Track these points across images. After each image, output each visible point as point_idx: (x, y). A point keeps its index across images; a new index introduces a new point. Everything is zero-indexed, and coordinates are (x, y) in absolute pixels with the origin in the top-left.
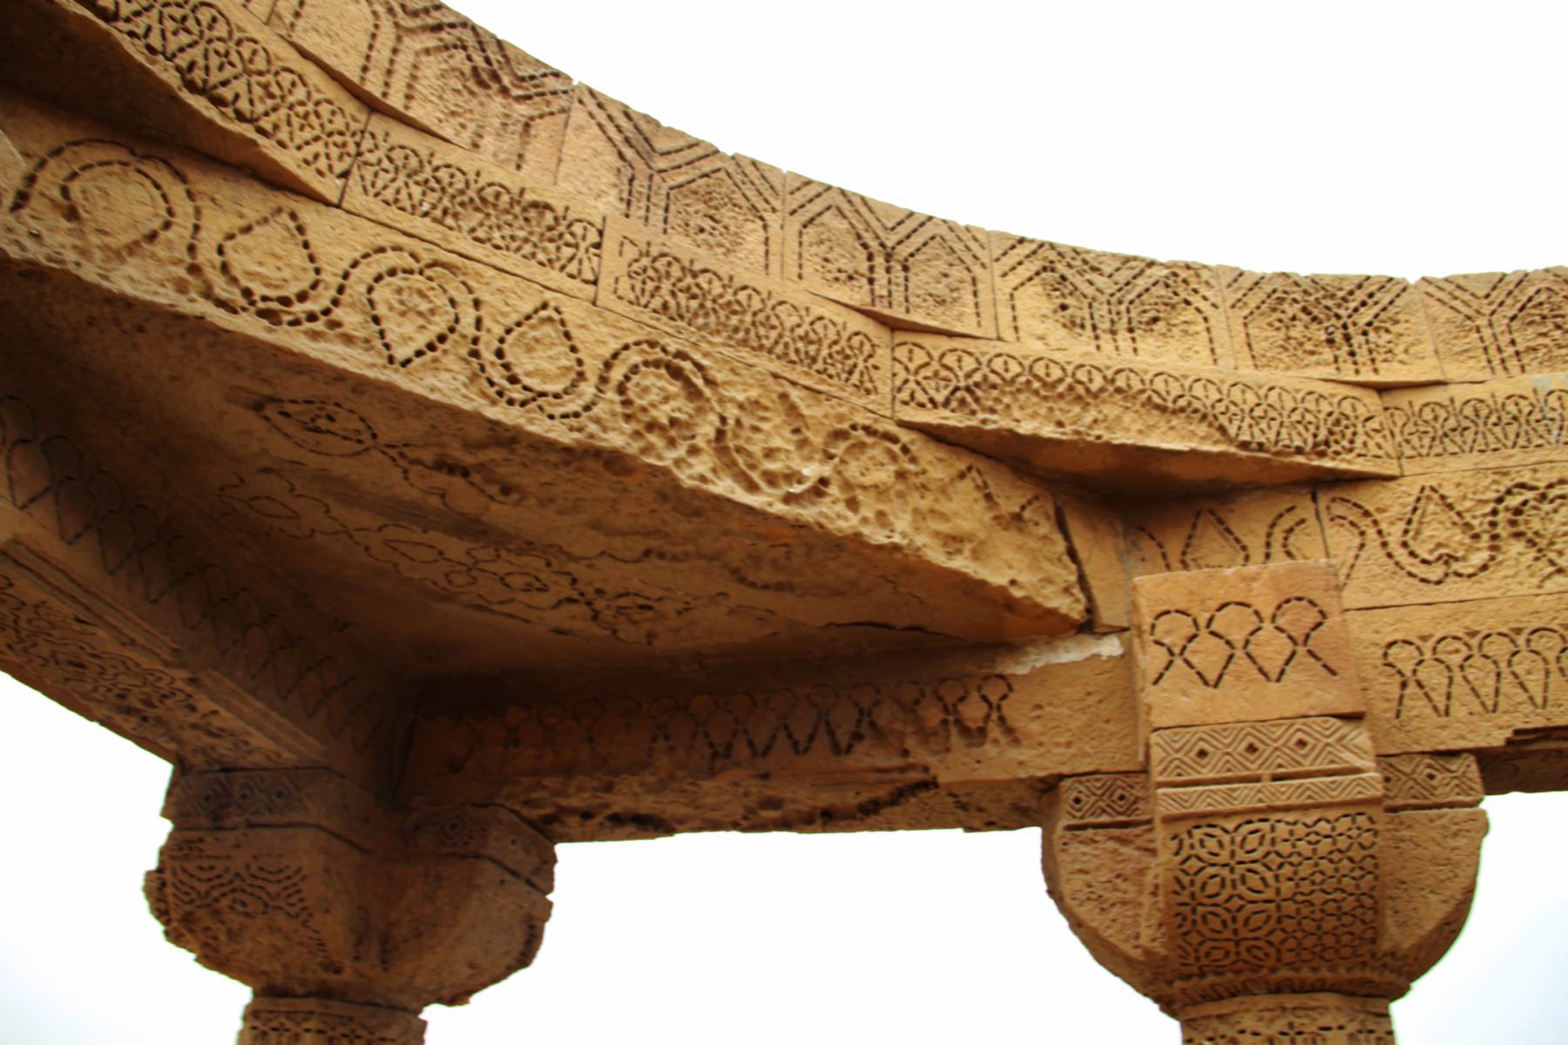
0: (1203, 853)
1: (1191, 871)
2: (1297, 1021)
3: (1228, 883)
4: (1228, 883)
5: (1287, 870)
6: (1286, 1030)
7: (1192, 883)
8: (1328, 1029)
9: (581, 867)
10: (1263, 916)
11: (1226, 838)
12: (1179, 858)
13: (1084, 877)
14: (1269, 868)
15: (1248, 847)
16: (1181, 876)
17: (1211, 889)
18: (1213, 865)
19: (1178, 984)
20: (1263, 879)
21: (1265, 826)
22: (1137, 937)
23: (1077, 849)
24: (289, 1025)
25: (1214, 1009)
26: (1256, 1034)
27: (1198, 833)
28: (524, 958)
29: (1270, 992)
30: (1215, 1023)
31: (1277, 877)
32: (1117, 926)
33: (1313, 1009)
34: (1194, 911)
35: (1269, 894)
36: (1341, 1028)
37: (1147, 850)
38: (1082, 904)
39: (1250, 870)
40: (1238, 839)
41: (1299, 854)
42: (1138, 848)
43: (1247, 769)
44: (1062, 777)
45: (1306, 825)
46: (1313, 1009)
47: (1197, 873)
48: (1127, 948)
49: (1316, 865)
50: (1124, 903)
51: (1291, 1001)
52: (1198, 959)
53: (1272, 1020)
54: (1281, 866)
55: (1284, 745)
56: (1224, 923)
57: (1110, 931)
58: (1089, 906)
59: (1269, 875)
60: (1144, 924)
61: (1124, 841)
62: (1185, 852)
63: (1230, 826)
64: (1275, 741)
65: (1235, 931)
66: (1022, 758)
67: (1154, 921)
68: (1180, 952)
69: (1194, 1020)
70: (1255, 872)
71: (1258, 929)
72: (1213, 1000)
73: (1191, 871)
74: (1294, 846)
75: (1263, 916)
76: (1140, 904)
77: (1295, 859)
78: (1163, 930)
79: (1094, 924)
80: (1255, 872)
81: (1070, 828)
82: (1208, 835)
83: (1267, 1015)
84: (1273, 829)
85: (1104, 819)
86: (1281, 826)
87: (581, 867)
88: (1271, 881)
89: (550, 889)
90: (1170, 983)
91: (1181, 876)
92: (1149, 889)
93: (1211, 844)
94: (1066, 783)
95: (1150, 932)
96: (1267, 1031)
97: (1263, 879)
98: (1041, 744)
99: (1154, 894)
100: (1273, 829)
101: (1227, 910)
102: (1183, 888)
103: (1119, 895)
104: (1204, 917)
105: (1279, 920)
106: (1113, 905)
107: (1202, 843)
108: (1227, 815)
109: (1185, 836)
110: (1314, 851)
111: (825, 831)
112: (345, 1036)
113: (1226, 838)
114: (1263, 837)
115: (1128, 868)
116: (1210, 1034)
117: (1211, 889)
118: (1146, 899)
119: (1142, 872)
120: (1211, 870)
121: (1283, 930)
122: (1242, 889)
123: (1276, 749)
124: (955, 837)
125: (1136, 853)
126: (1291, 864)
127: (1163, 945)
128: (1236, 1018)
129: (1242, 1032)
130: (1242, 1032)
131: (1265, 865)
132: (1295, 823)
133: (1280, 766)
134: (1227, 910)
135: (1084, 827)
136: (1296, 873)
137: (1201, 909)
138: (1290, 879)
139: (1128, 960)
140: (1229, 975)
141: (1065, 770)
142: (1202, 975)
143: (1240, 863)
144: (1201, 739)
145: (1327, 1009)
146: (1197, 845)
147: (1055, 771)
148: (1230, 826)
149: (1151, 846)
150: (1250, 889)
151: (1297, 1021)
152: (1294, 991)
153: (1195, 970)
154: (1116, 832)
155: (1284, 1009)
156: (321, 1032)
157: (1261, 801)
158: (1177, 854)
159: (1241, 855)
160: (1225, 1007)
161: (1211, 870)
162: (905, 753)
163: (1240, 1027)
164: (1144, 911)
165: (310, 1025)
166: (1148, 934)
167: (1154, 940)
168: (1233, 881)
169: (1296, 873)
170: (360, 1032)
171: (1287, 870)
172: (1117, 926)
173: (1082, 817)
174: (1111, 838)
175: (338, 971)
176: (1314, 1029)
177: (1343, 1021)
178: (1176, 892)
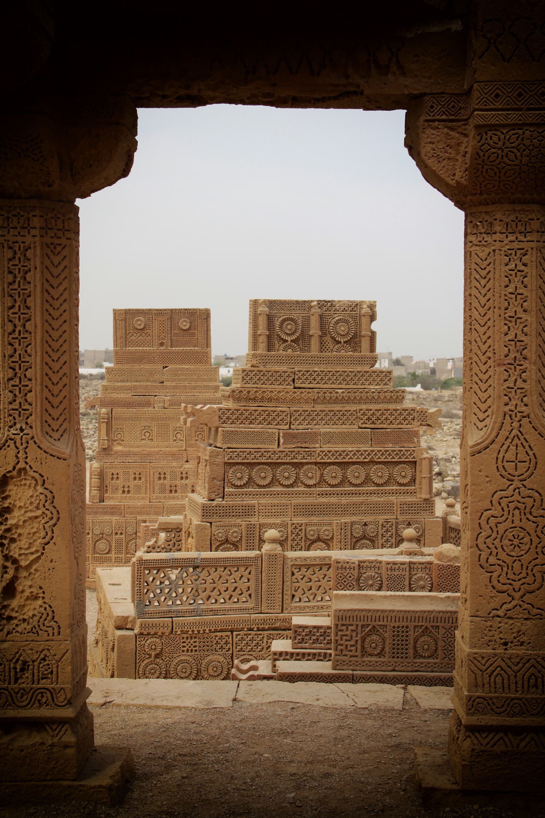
0: (491, 142)
1: (484, 150)
2: (519, 216)
3: (500, 156)
4: (500, 156)
5: (526, 152)
6: (515, 219)
7: (484, 155)
8: (533, 220)
9: (153, 123)
10: (513, 171)
11: (502, 137)
12: (479, 144)
13: (431, 145)
14: (519, 151)
15: (511, 141)
16: (480, 152)
17: (491, 159)
18: (495, 148)
19: (469, 197)
20: (515, 155)
21: (521, 132)
22: (454, 175)
23: (429, 131)
24: (22, 213)
25: (483, 209)
26: (501, 221)
27: (490, 133)
28: (125, 173)
29: (510, 203)
30: (484, 215)
31: (522, 155)
32: (445, 169)
33: (528, 211)
34: (483, 167)
35: (517, 162)
36: (538, 219)
37: (462, 134)
38: (429, 158)
39: (510, 151)
40: (507, 137)
41: (533, 145)
42: (458, 133)
43: (516, 104)
44: (425, 94)
45: (538, 132)
46: (528, 211)
47: (502, 169)
48: (449, 180)
49: (540, 150)
50: (449, 159)
51: (518, 207)
52: (480, 187)
53: (509, 215)
54: (524, 150)
55: (535, 94)
56: (495, 173)
57: (441, 172)
58: (433, 159)
59: (518, 154)
60: (458, 170)
61: (452, 129)
62: (483, 141)
63: (505, 131)
64: (531, 92)
65: (500, 177)
66: (406, 83)
67: (463, 169)
68: (474, 184)
69: (474, 213)
70: (513, 153)
71: (510, 176)
72: (484, 205)
73: (484, 150)
74: (531, 142)
75: (513, 171)
76: (457, 160)
77: (530, 148)
78: (467, 173)
79: (434, 168)
80: (513, 153)
81: (427, 121)
82: (494, 134)
83: (507, 213)
84: (524, 133)
85: (444, 117)
86: (527, 132)
87: (157, 127)
88: (519, 157)
89: (136, 135)
90: (466, 196)
91: (480, 152)
92: (462, 153)
93: (495, 138)
94: (427, 98)
95: (461, 174)
96: (506, 220)
97: (515, 155)
98: (416, 76)
99: (464, 156)
100: (524, 133)
101: (498, 168)
102: (479, 157)
103: (448, 155)
104: (487, 170)
105: (520, 174)
106: (444, 160)
107: (491, 137)
108: (504, 126)
109: (484, 135)
110: (540, 144)
111: (291, 107)
112: (52, 218)
113: (502, 137)
114: (519, 136)
115: (453, 142)
116: (481, 220)
117: (491, 159)
118: (460, 158)
119: (459, 144)
120: (493, 150)
121: (520, 178)
122: (505, 159)
123: (532, 96)
124: (360, 112)
125: (457, 135)
126: (529, 150)
127: (466, 180)
128: (494, 213)
129: (496, 220)
130: (496, 220)
131: (517, 149)
132: (533, 132)
133: (532, 104)
134: (498, 168)
135: (434, 121)
136: (530, 154)
137: (486, 167)
138: (527, 156)
139: (448, 185)
140: (493, 195)
141: (427, 91)
142: (481, 194)
143: (506, 148)
144: (498, 88)
145: (533, 211)
146: (489, 139)
147: (423, 92)
148: (505, 131)
149: (466, 132)
150: (509, 159)
151: (519, 216)
152: (520, 203)
153: (479, 192)
154: (449, 124)
155: (515, 211)
156: (41, 216)
157: (520, 120)
158: (479, 142)
159: (508, 144)
160: (489, 209)
161: (493, 150)
162: (348, 77)
163: (494, 217)
164: (458, 163)
165: (37, 213)
166: (459, 175)
167: (462, 178)
168: (502, 156)
169: (530, 154)
170: (59, 216)
171: (526, 152)
172: (445, 169)
173: (433, 116)
174: (446, 127)
175: (50, 186)
176: (527, 219)
177: (539, 217)
178: (476, 159)
